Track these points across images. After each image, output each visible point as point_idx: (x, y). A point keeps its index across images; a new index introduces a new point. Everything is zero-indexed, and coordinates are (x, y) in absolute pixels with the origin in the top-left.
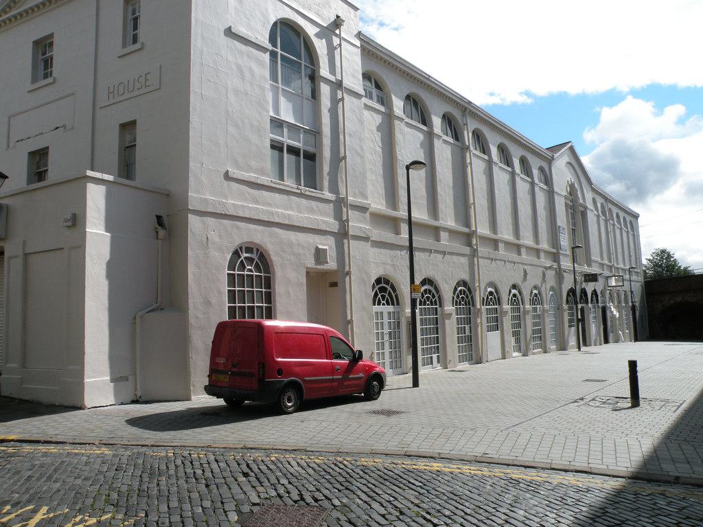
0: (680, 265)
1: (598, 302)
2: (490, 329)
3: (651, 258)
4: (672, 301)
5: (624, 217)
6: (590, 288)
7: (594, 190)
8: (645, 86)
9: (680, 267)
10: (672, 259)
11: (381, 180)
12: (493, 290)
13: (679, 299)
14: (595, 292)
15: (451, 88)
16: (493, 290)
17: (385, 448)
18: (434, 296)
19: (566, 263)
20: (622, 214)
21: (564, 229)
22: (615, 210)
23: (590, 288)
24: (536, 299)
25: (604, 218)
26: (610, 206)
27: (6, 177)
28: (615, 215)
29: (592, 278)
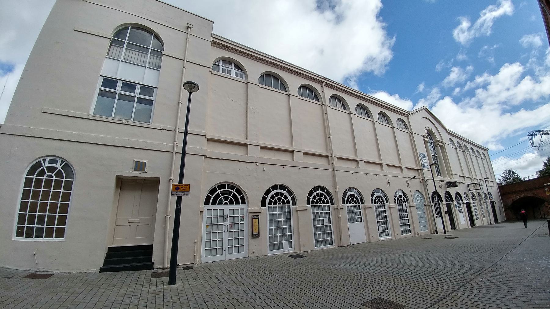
0: (520, 178)
1: (462, 200)
2: (351, 220)
3: (503, 175)
4: (518, 197)
5: (482, 152)
6: (453, 191)
7: (448, 133)
8: (450, 74)
9: (521, 178)
10: (516, 175)
11: (376, 148)
12: (402, 195)
13: (522, 196)
14: (458, 194)
15: (333, 80)
16: (402, 195)
17: (386, 298)
18: (325, 198)
19: (428, 175)
20: (475, 149)
21: (424, 155)
22: (469, 146)
23: (453, 191)
24: (402, 199)
25: (468, 153)
26: (464, 143)
27: (1, 127)
28: (476, 152)
29: (453, 184)
